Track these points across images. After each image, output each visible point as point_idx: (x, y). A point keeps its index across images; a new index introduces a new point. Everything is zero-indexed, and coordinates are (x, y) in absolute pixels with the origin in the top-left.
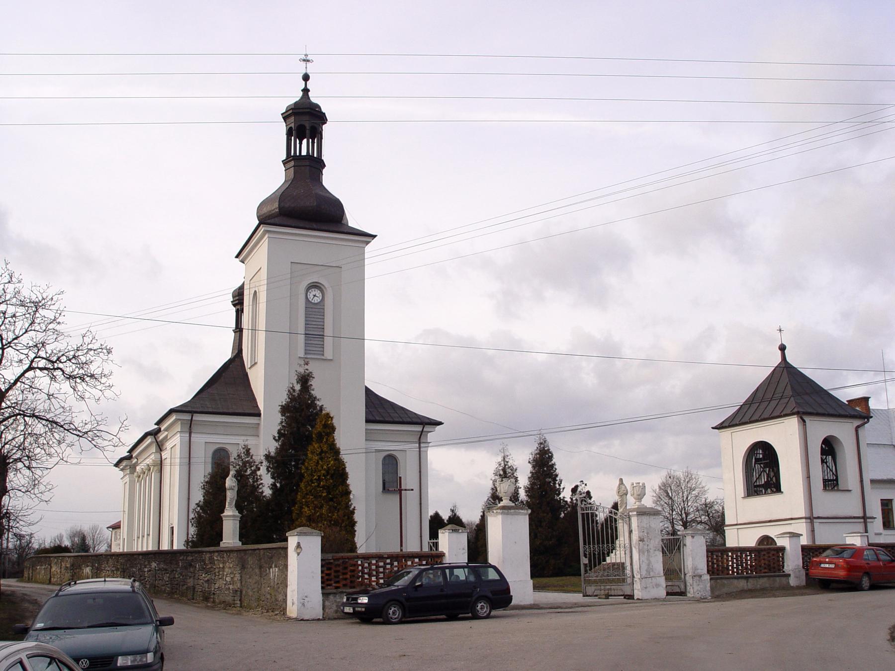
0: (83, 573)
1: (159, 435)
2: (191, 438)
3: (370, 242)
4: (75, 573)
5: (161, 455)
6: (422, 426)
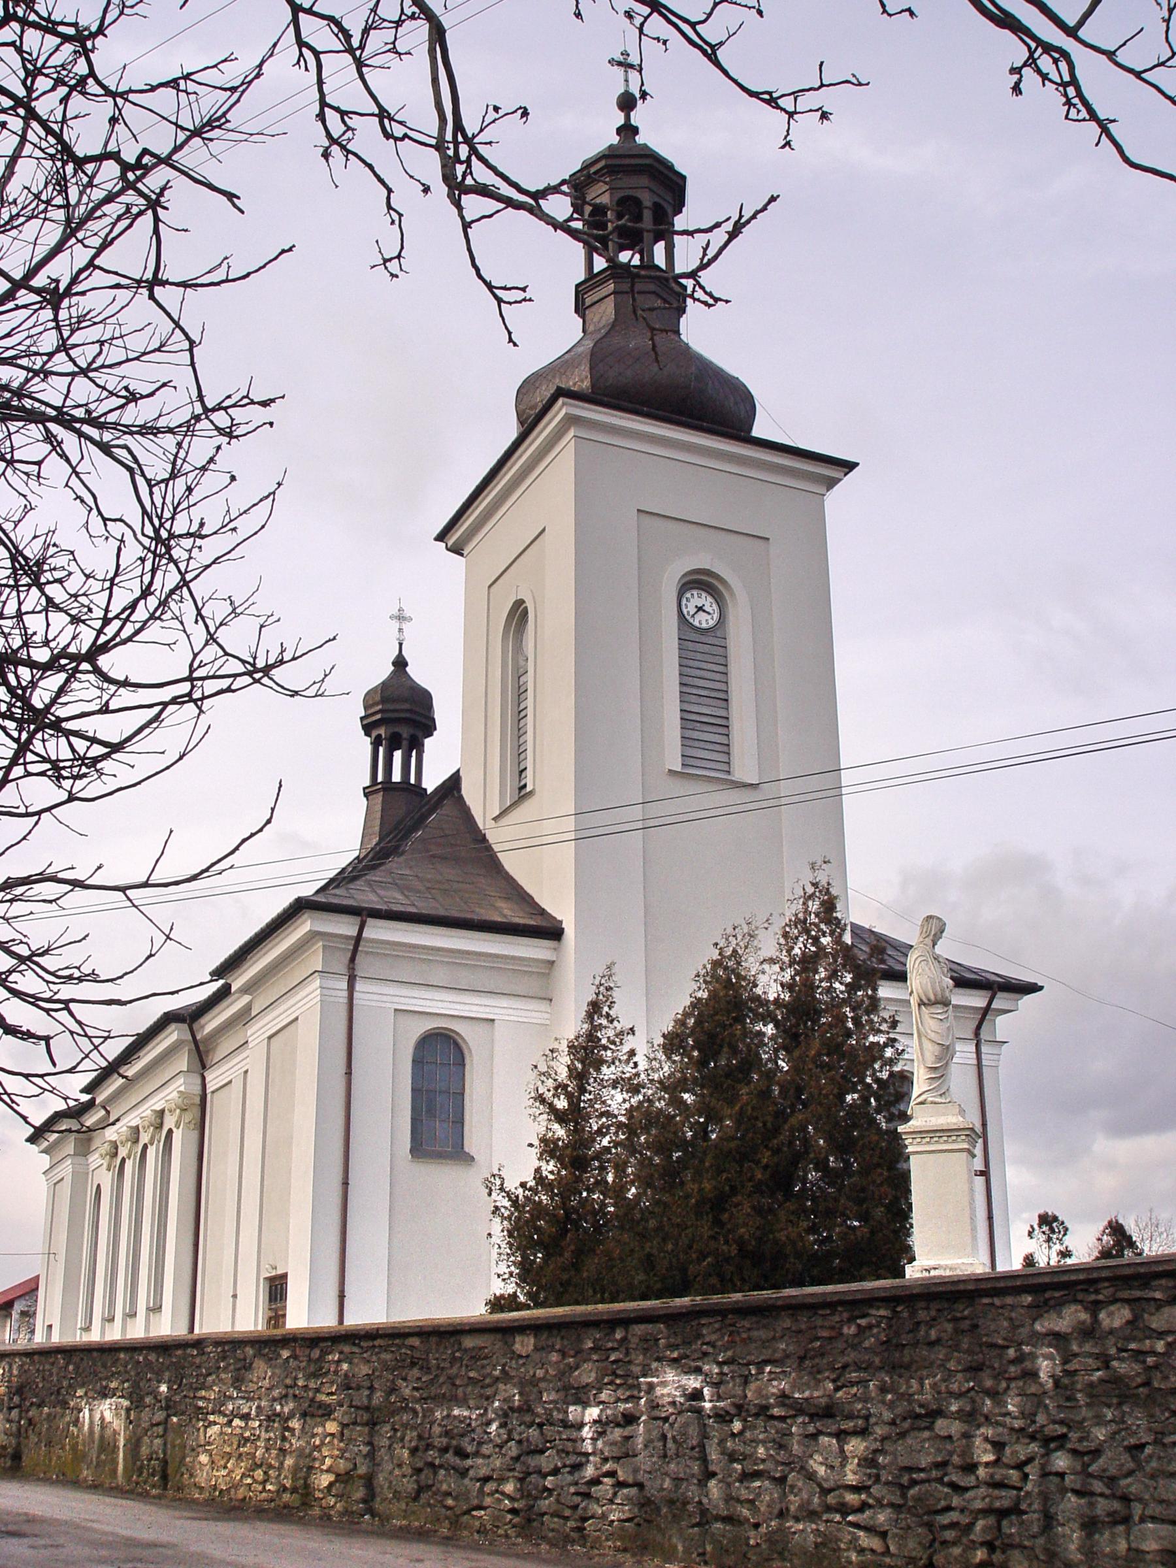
0: (76, 1422)
1: (202, 1021)
2: (356, 995)
3: (837, 481)
4: (30, 1422)
5: (203, 1078)
6: (988, 994)
